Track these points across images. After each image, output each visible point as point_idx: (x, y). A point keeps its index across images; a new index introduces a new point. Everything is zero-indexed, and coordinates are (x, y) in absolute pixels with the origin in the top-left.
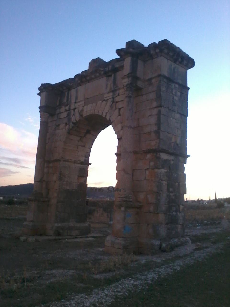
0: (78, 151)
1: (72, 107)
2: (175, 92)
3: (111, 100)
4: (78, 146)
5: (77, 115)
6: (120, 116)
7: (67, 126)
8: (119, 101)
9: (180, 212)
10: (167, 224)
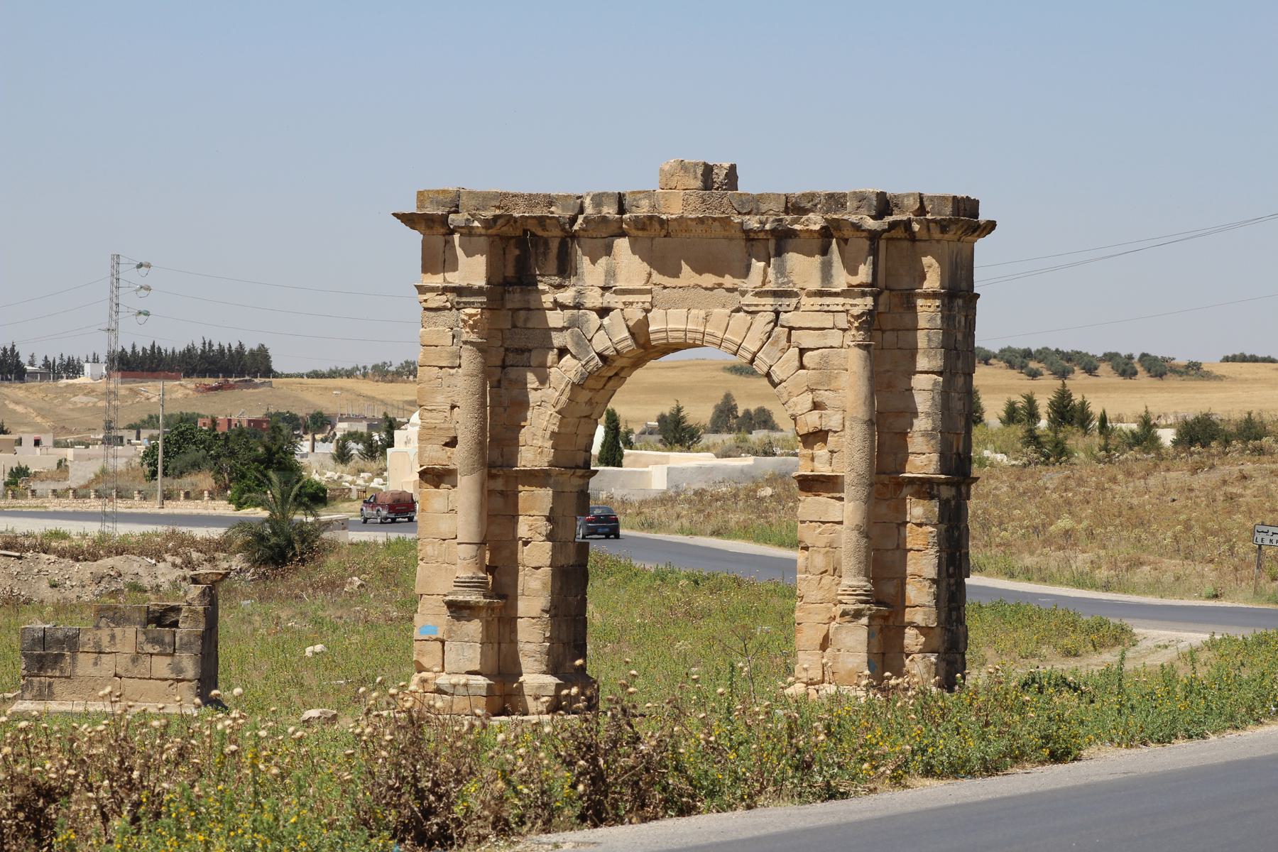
8: (800, 328)
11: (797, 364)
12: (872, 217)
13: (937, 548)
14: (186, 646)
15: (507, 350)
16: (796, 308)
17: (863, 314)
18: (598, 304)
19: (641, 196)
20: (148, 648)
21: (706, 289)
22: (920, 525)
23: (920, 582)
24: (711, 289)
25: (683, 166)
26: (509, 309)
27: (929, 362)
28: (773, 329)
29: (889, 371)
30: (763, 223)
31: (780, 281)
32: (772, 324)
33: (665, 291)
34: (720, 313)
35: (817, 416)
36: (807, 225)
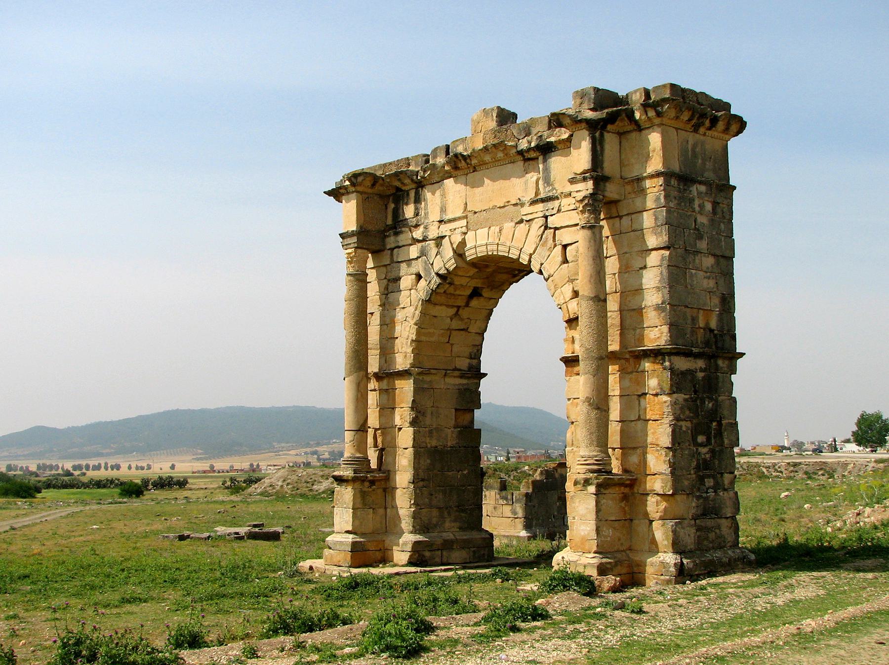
0: (452, 345)
1: (433, 233)
2: (699, 206)
3: (541, 221)
4: (450, 333)
5: (448, 252)
6: (566, 265)
7: (423, 283)
8: (562, 227)
9: (725, 490)
10: (695, 518)
11: (560, 259)
12: (591, 109)
13: (671, 418)
14: (518, 501)
15: (389, 280)
16: (559, 211)
17: (585, 197)
18: (436, 235)
19: (458, 143)
20: (501, 502)
21: (500, 207)
22: (656, 395)
23: (658, 450)
24: (503, 207)
25: (486, 112)
26: (389, 249)
27: (657, 239)
28: (544, 232)
29: (626, 253)
30: (529, 142)
31: (547, 189)
32: (543, 227)
33: (476, 215)
34: (509, 226)
35: (575, 304)
36: (559, 136)
